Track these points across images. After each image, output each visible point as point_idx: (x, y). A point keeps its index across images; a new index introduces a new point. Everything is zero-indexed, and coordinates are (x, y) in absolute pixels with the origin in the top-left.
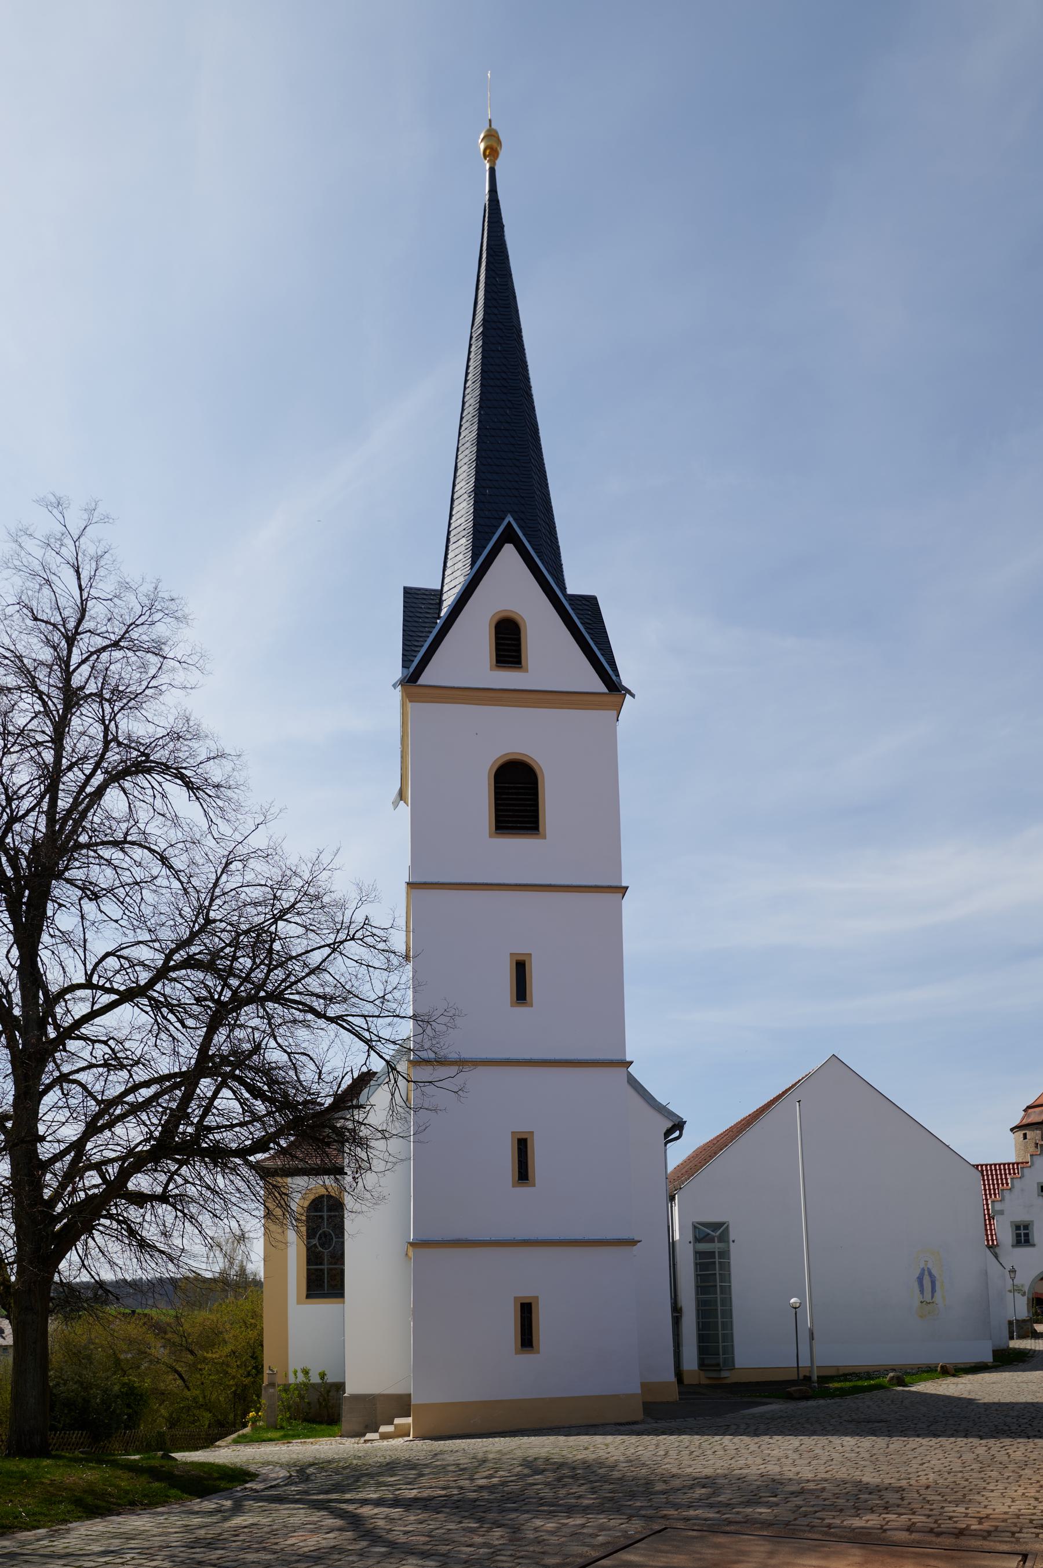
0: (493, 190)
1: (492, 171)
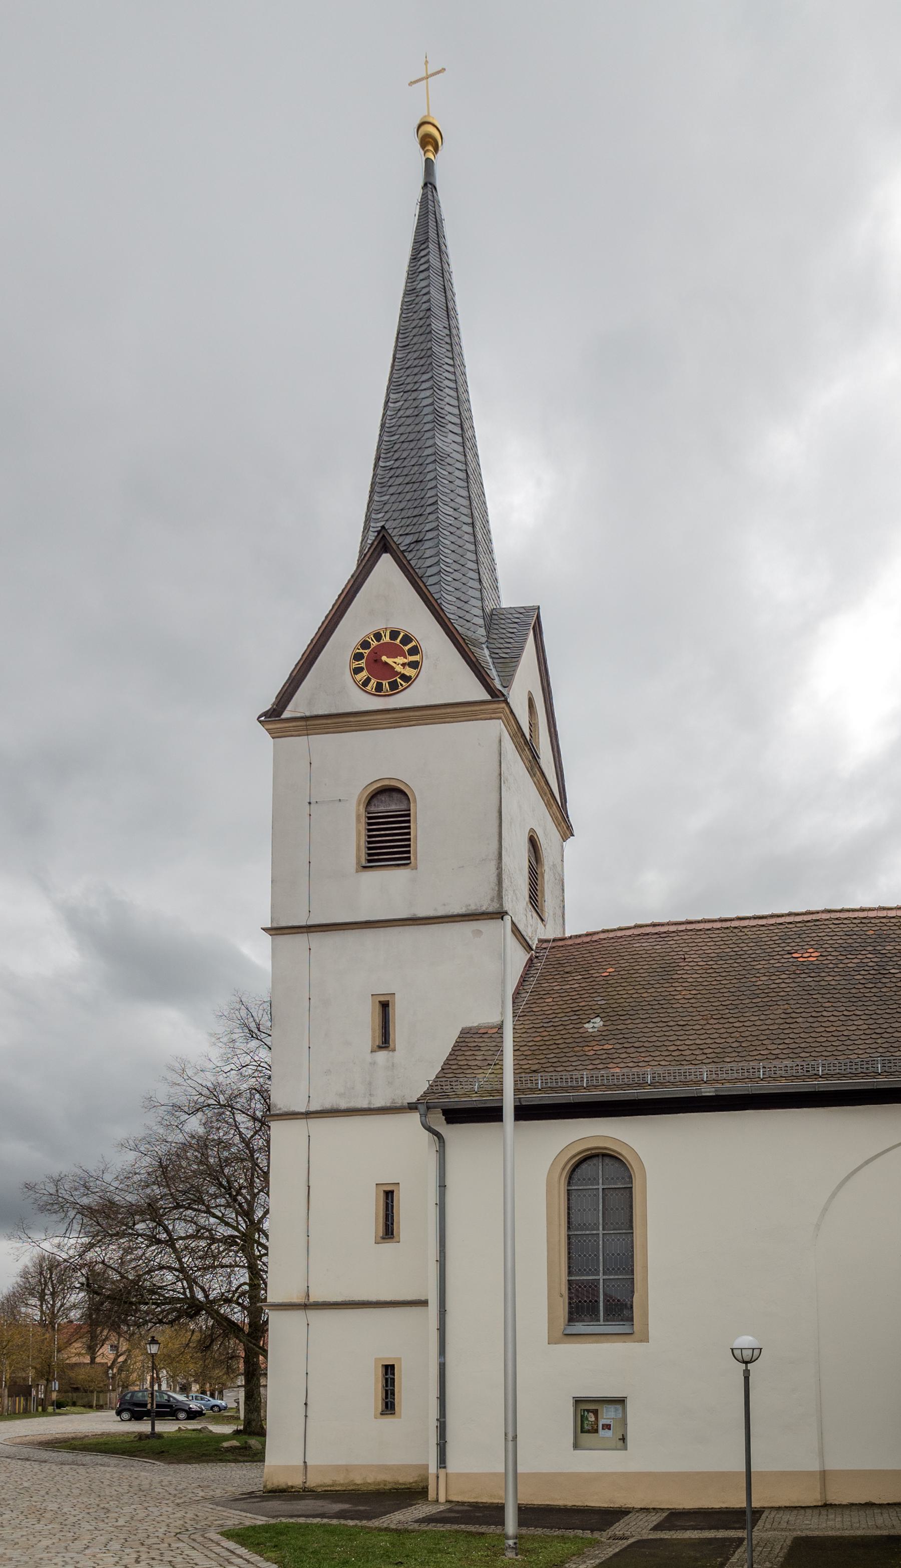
0: (429, 185)
1: (429, 165)
